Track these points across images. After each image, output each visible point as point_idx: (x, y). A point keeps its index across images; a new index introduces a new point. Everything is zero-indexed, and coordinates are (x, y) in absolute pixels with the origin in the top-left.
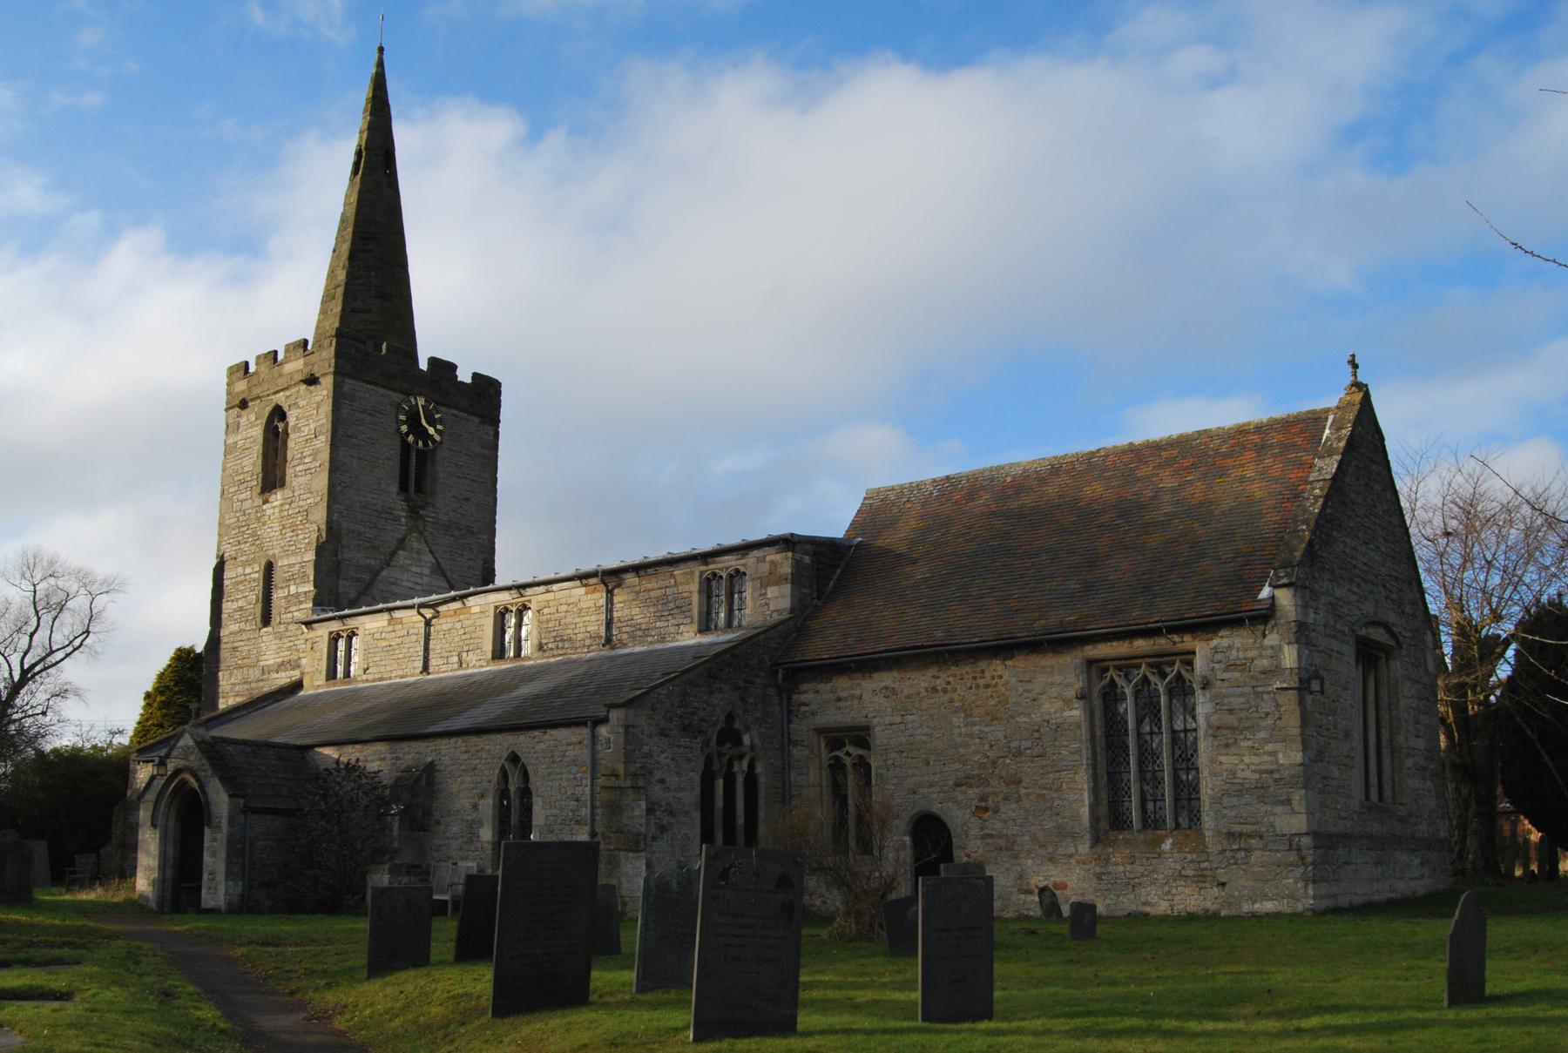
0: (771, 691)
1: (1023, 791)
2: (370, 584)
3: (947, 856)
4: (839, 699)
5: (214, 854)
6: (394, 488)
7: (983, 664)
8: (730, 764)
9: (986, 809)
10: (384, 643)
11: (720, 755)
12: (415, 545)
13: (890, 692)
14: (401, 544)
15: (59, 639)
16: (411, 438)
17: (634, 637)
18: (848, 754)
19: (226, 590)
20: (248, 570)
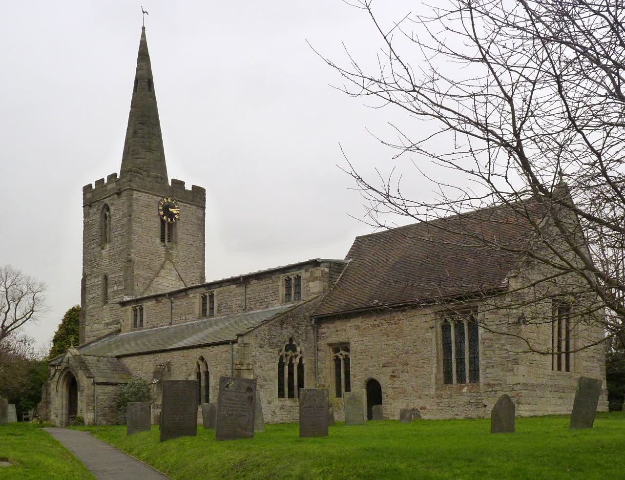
0: (309, 328)
1: (409, 369)
2: (149, 285)
3: (76, 412)
4: (337, 331)
5: (82, 402)
6: (158, 241)
7: (394, 314)
8: (291, 360)
9: (395, 376)
10: (154, 312)
11: (287, 356)
12: (169, 267)
13: (357, 327)
14: (162, 267)
15: (19, 315)
16: (165, 218)
17: (256, 307)
18: (341, 354)
19: (88, 289)
20: (96, 280)
